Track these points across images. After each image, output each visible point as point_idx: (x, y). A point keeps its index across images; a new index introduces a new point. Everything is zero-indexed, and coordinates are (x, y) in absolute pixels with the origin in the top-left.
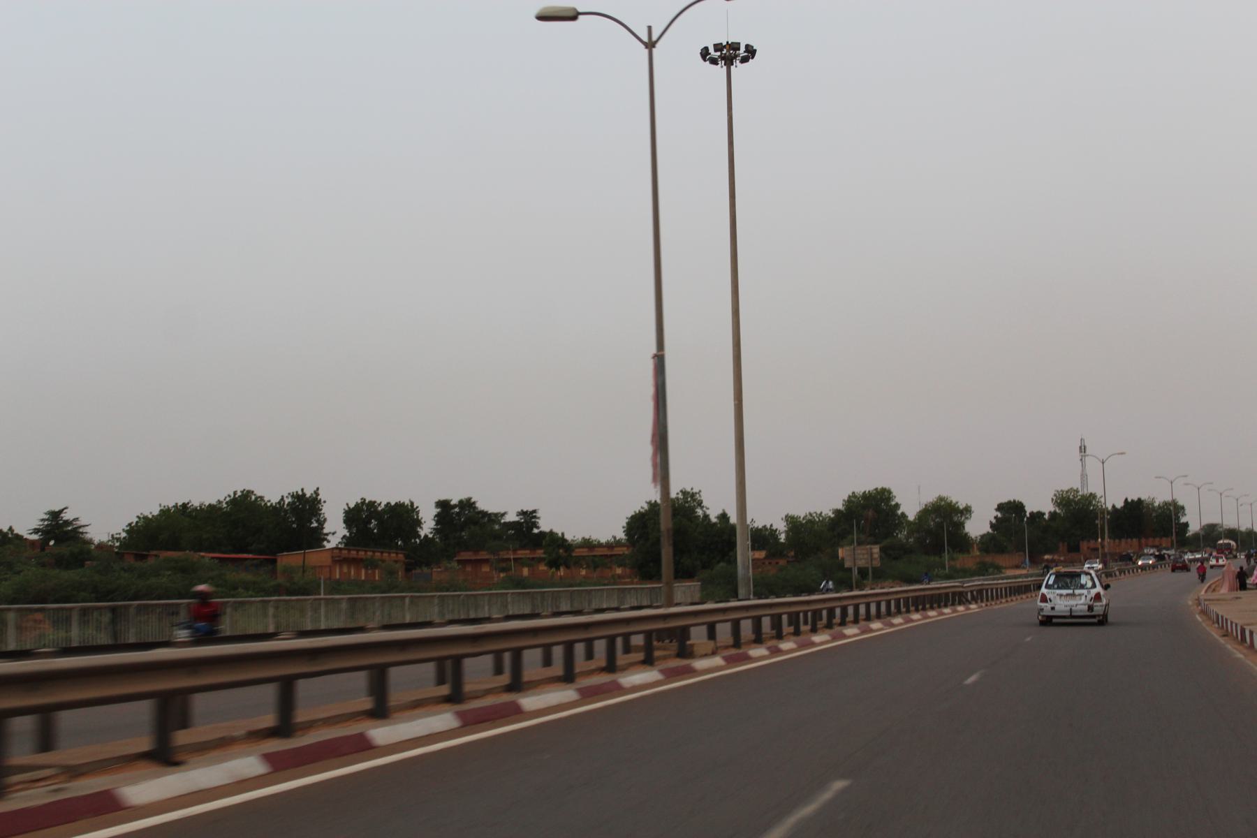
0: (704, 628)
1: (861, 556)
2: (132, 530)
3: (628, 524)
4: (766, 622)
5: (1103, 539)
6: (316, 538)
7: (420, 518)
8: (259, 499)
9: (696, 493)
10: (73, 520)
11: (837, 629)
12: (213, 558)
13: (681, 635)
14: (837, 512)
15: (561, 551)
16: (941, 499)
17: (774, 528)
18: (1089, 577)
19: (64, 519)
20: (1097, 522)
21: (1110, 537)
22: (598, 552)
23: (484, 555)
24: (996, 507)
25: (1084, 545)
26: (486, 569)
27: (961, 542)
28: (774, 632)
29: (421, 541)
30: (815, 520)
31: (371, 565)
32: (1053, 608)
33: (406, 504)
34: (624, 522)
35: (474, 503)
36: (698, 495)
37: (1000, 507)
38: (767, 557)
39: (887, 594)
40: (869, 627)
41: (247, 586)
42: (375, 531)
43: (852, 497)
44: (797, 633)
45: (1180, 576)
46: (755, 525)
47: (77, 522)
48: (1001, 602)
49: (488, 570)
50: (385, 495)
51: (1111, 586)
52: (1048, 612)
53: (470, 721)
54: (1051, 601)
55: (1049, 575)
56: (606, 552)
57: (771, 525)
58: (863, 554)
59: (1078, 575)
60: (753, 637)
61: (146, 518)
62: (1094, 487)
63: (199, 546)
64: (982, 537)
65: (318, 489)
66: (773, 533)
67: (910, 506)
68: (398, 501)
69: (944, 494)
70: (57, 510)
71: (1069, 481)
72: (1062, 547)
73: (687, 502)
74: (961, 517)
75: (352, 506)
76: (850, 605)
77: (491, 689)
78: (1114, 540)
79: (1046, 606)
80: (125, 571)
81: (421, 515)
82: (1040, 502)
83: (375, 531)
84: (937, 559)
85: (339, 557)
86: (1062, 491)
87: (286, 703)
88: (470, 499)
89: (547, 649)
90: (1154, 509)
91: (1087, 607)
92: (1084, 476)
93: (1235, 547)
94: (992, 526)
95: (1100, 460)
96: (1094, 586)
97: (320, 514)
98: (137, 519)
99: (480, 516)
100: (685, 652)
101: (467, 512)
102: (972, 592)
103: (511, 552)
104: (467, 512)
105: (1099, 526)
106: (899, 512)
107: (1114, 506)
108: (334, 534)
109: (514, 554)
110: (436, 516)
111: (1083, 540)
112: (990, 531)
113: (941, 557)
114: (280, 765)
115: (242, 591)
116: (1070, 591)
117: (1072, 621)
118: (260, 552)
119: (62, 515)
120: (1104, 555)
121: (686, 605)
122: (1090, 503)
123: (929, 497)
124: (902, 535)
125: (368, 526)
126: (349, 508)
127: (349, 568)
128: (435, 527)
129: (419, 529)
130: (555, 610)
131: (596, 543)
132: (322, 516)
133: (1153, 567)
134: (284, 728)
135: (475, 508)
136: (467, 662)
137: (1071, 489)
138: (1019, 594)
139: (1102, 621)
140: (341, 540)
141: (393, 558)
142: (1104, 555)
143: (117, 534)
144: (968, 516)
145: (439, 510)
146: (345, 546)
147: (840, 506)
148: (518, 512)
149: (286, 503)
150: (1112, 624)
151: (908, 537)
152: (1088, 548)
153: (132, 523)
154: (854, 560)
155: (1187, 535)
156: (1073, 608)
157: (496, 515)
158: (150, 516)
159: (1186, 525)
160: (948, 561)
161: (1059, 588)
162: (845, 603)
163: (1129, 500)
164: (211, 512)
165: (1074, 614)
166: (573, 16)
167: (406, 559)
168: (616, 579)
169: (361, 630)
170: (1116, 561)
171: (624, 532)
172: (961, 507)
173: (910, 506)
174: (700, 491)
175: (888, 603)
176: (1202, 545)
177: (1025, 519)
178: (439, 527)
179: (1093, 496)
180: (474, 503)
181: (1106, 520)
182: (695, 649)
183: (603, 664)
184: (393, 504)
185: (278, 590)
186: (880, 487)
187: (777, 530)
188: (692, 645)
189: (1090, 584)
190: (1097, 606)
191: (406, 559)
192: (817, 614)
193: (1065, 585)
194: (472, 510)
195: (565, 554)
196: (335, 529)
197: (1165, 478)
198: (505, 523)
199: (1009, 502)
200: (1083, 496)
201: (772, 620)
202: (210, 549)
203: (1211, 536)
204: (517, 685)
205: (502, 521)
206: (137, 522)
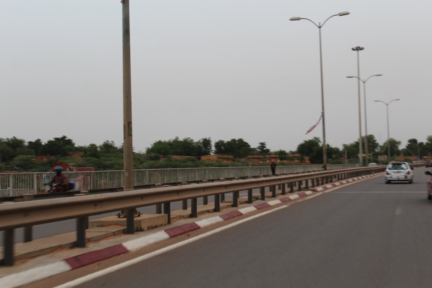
4: (267, 189)
37: (410, 141)
39: (204, 189)
59: (400, 164)
76: (304, 180)
89: (185, 201)
96: (407, 169)
117: (399, 182)
121: (238, 179)
139: (410, 182)
150: (415, 183)
157: (263, 143)
161: (394, 169)
162: (283, 182)
166: (299, 19)
183: (213, 207)
204: (194, 214)
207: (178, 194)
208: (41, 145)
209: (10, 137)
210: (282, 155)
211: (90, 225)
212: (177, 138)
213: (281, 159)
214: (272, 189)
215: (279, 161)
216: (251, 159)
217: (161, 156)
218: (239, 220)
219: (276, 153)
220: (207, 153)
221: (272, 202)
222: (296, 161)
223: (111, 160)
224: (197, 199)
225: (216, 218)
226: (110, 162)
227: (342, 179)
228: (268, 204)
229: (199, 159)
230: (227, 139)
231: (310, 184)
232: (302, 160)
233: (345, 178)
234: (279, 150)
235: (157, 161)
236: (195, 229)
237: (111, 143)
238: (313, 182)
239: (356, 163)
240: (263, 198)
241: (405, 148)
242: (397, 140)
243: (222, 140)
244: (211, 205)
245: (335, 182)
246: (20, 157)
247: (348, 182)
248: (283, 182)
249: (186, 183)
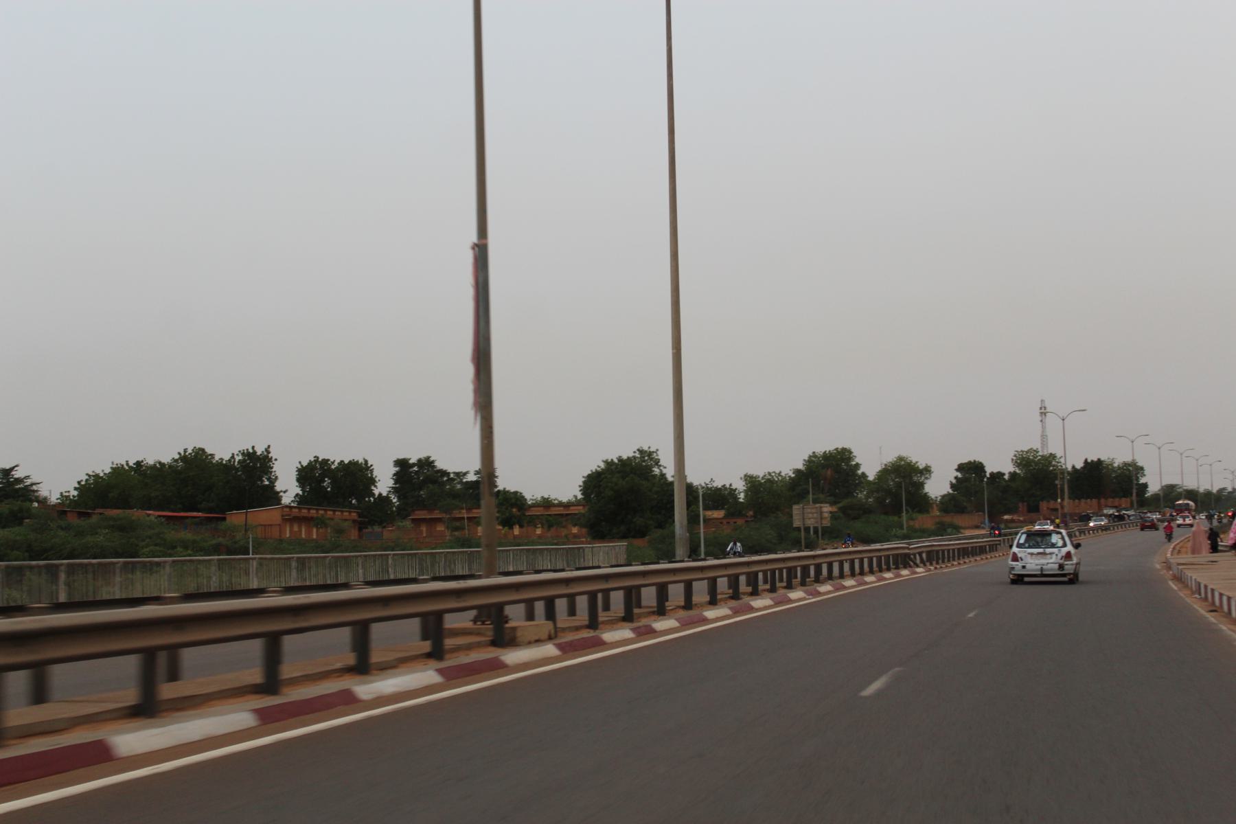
0: (522, 606)
1: (810, 515)
2: (83, 489)
3: (584, 482)
4: (722, 583)
5: (1063, 499)
6: (271, 496)
7: (374, 476)
8: (209, 457)
9: (653, 452)
10: (24, 478)
11: (746, 599)
12: (160, 516)
14: (797, 472)
15: (514, 510)
16: (901, 459)
17: (734, 487)
18: (1059, 536)
19: (16, 476)
20: (1057, 482)
21: (1070, 498)
22: (554, 511)
23: (437, 514)
24: (956, 467)
25: (1044, 506)
26: (440, 528)
27: (920, 502)
28: (731, 591)
29: (375, 499)
30: (774, 480)
31: (320, 523)
32: (1024, 567)
33: (360, 462)
34: (580, 481)
35: (433, 462)
36: (655, 454)
37: (961, 468)
38: (725, 517)
39: (567, 582)
40: (864, 581)
41: (185, 545)
42: (329, 489)
43: (813, 457)
44: (773, 589)
45: (1149, 534)
46: (715, 485)
47: (28, 480)
48: (953, 565)
49: (443, 529)
50: (338, 453)
51: (1082, 544)
52: (1018, 571)
53: (453, 676)
54: (1022, 560)
55: (1020, 535)
56: (561, 510)
57: (731, 485)
58: (813, 513)
60: (707, 598)
61: (97, 476)
62: (1054, 448)
63: (147, 504)
64: (943, 497)
65: (269, 447)
66: (732, 492)
67: (870, 466)
68: (351, 459)
69: (904, 454)
70: (8, 468)
71: (1029, 442)
72: (1022, 507)
73: (644, 461)
74: (921, 476)
75: (305, 464)
76: (856, 558)
77: (97, 714)
78: (1074, 500)
80: (62, 529)
81: (375, 474)
82: (1000, 462)
83: (329, 489)
84: (896, 518)
85: (289, 515)
86: (1022, 451)
87: (273, 658)
88: (429, 457)
90: (1113, 470)
91: (1057, 565)
92: (1044, 437)
93: (1194, 508)
94: (952, 486)
95: (1060, 417)
96: (1065, 545)
97: (271, 472)
98: (87, 477)
99: (439, 474)
101: (425, 471)
102: (920, 554)
103: (464, 511)
104: (425, 471)
105: (1059, 486)
106: (860, 472)
107: (1073, 467)
108: (285, 492)
109: (467, 513)
110: (394, 475)
111: (1042, 501)
112: (951, 491)
113: (900, 517)
114: (269, 719)
115: (181, 550)
116: (1041, 550)
117: (1043, 579)
118: (210, 510)
119: (13, 473)
120: (1064, 515)
122: (1050, 463)
123: (889, 457)
124: (861, 495)
125: (322, 485)
126: (302, 466)
127: (300, 527)
128: (394, 486)
129: (373, 488)
131: (556, 502)
132: (273, 474)
133: (1104, 529)
135: (434, 467)
136: (376, 628)
137: (1031, 449)
138: (973, 556)
139: (1073, 579)
140: (293, 499)
141: (343, 517)
142: (1064, 515)
143: (66, 492)
144: (927, 476)
145: (397, 469)
146: (298, 504)
147: (800, 466)
148: (476, 471)
149: (237, 460)
150: (1083, 583)
151: (868, 497)
152: (1048, 508)
153: (82, 481)
154: (804, 519)
155: (1146, 496)
156: (1044, 567)
158: (102, 475)
159: (1145, 486)
160: (907, 521)
161: (1030, 547)
162: (711, 574)
163: (1089, 461)
164: (159, 471)
167: (359, 517)
168: (570, 539)
169: (346, 586)
170: (1075, 521)
171: (580, 491)
172: (921, 467)
173: (870, 466)
174: (657, 450)
175: (871, 560)
176: (1162, 506)
177: (985, 480)
178: (397, 486)
179: (1053, 456)
180: (433, 462)
181: (1066, 480)
182: (519, 634)
184: (346, 462)
185: (217, 550)
186: (840, 447)
187: (736, 489)
188: (514, 629)
189: (1060, 543)
190: (1067, 565)
191: (359, 517)
192: (791, 572)
193: (1035, 544)
194: (430, 469)
195: (518, 513)
196: (288, 487)
197: (1127, 438)
198: (467, 482)
199: (970, 463)
200: (1042, 456)
201: (728, 579)
202: (159, 507)
203: (1170, 495)
205: (464, 480)
206: (87, 480)
207: (702, 572)
211: (635, 617)
218: (689, 629)
225: (625, 633)
228: (704, 616)
240: (842, 576)
248: (755, 569)
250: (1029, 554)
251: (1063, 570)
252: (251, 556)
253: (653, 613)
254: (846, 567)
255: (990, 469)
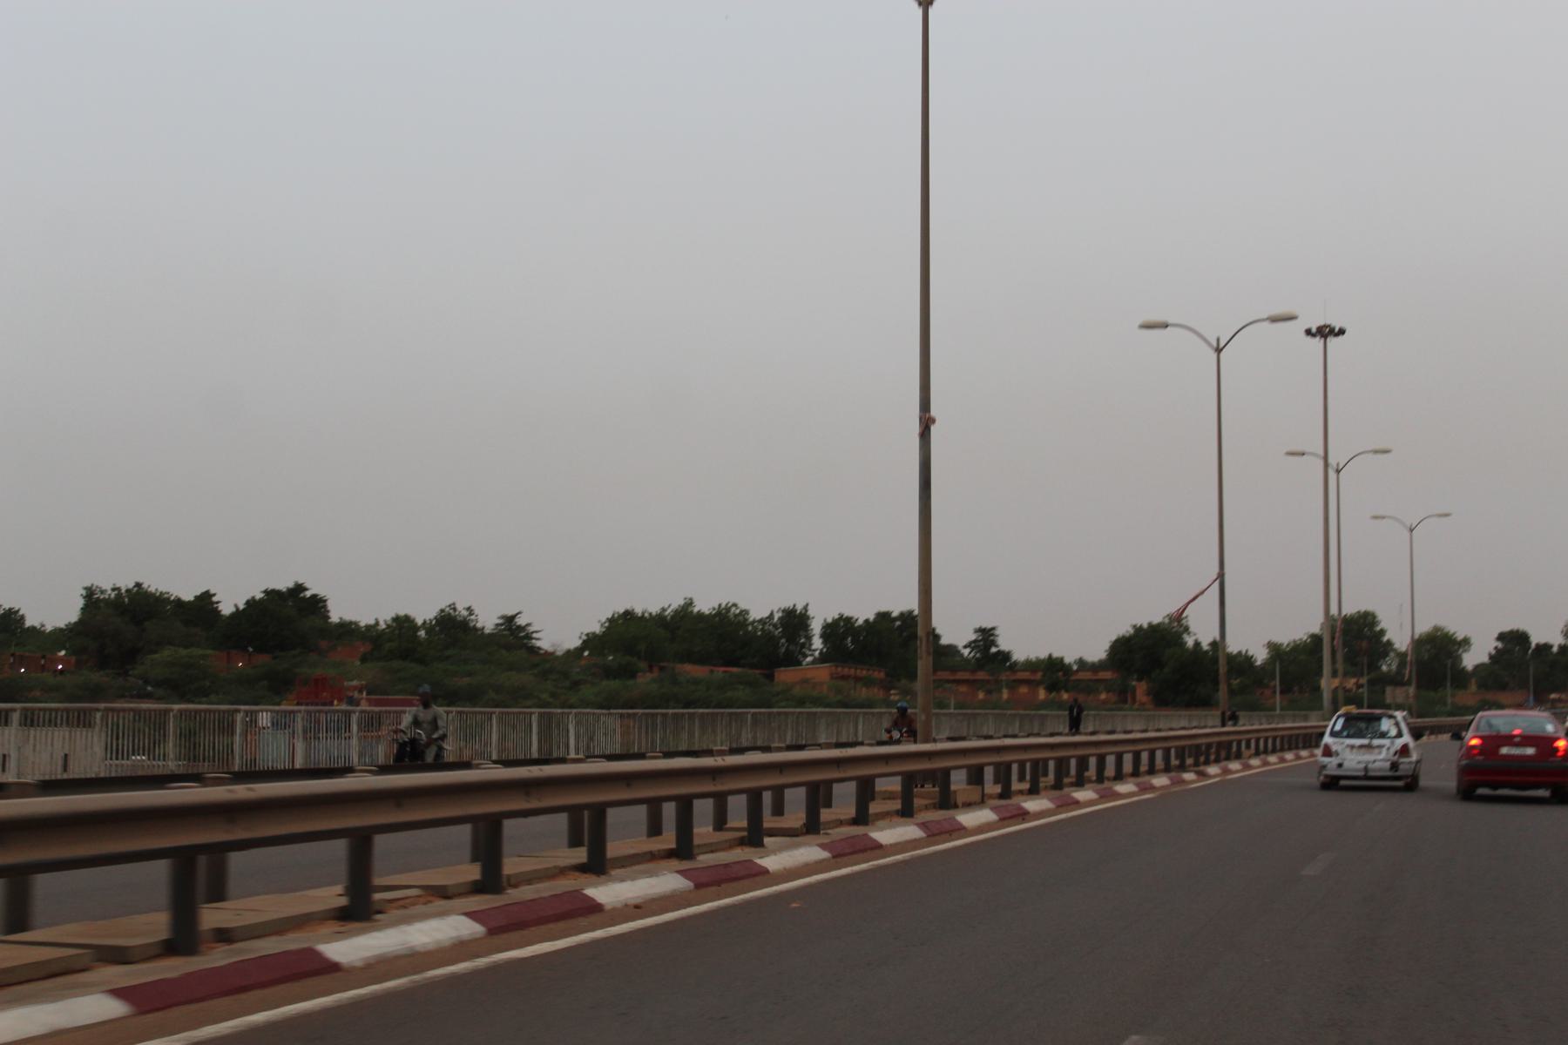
0: (641, 811)
13: (942, 778)
16: (1437, 629)
18: (1392, 721)
19: (518, 624)
52: (1332, 770)
59: (1378, 718)
65: (807, 605)
67: (1400, 636)
76: (1159, 748)
79: (1331, 762)
89: (654, 805)
96: (1400, 735)
100: (946, 801)
110: (22, 617)
130: (734, 746)
134: (182, 940)
136: (381, 842)
144: (1466, 647)
156: (1370, 766)
161: (1348, 736)
162: (1103, 750)
165: (1371, 774)
173: (1400, 636)
186: (1363, 610)
189: (1394, 732)
190: (1402, 763)
199: (1511, 632)
201: (749, 801)
207: (714, 779)
208: (217, 612)
209: (126, 583)
210: (1052, 672)
211: (870, 819)
212: (690, 603)
213: (1053, 687)
214: (976, 776)
215: (1042, 694)
216: (948, 686)
217: (643, 665)
219: (1031, 666)
220: (792, 660)
221: (1032, 805)
222: (1103, 696)
223: (470, 674)
224: (761, 794)
225: (809, 852)
226: (467, 680)
227: (1266, 752)
229: (771, 677)
230: (863, 613)
231: (1128, 766)
232: (1124, 696)
233: (1274, 751)
234: (1043, 655)
235: (631, 682)
236: (959, 829)
237: (465, 613)
238: (1167, 758)
239: (1312, 709)
241: (1485, 659)
242: (1458, 630)
243: (847, 613)
244: (795, 816)
245: (1250, 757)
246: (166, 653)
247: (1282, 760)
249: (661, 754)
250: (1348, 746)
251: (1396, 771)
252: (952, 711)
253: (979, 804)
254: (1128, 760)
255: (1536, 639)
